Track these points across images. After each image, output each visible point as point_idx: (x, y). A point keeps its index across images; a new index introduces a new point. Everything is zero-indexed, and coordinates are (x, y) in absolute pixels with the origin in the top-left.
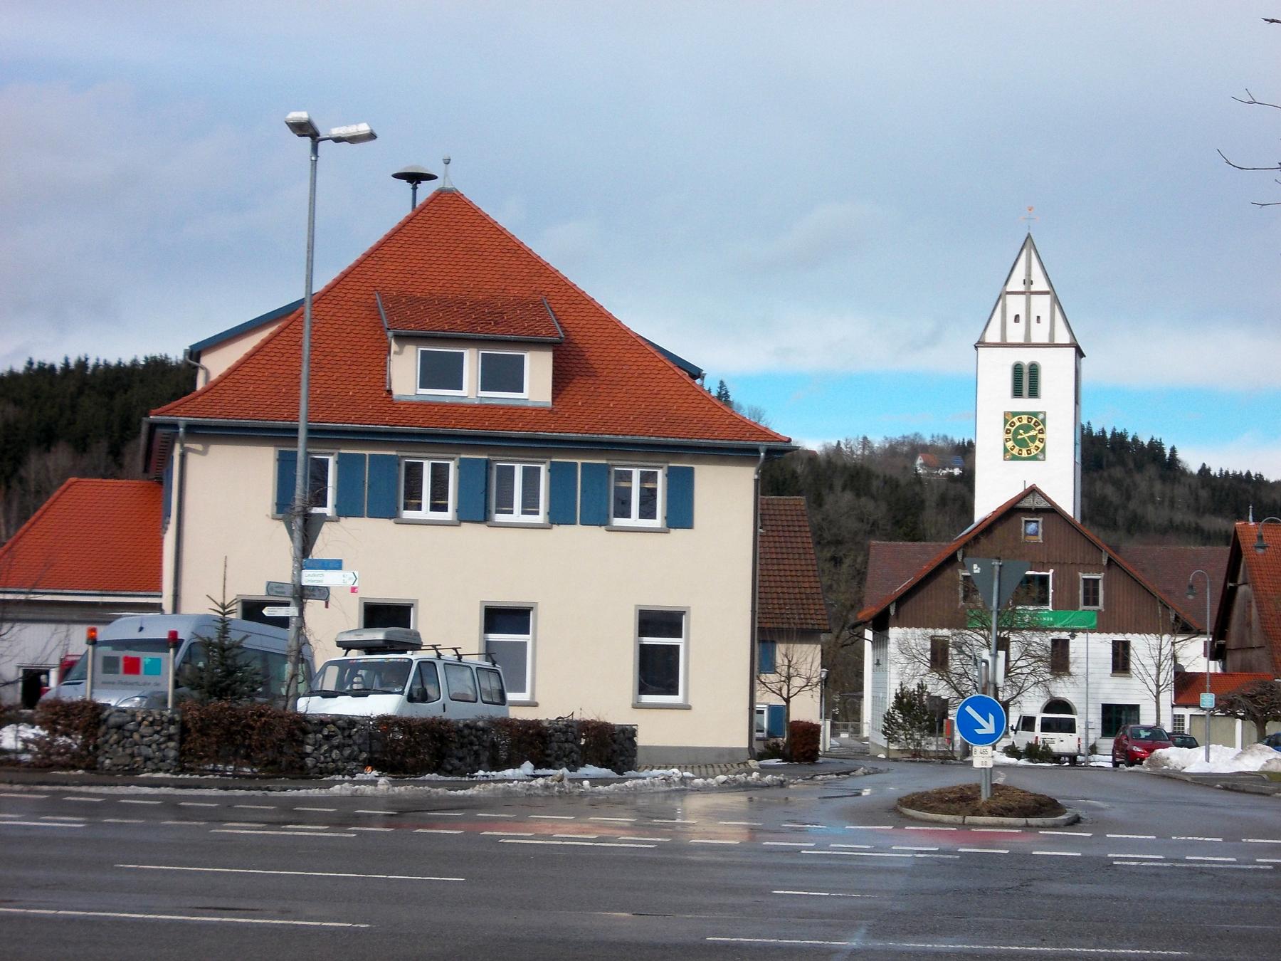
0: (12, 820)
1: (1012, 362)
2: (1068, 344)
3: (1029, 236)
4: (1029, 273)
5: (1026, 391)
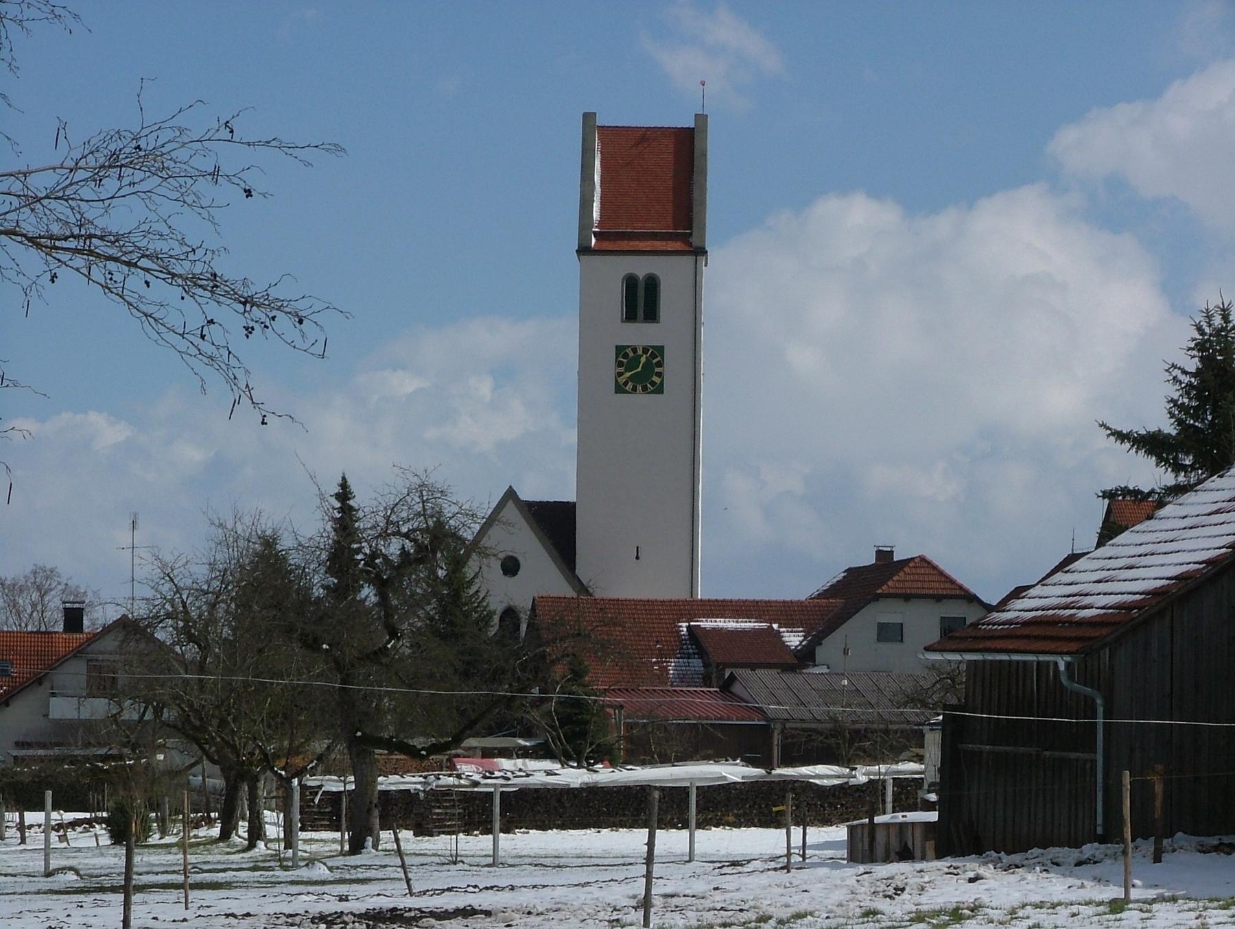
5: (640, 313)
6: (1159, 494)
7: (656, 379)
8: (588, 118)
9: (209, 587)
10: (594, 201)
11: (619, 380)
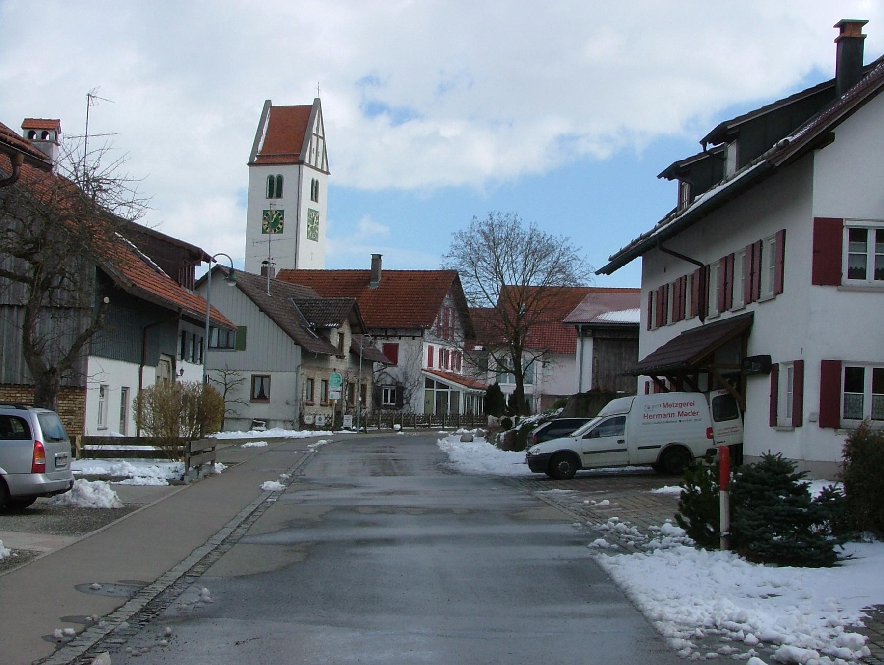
1: (267, 175)
5: (275, 194)
6: (62, 258)
7: (280, 226)
8: (268, 102)
9: (494, 358)
10: (260, 141)
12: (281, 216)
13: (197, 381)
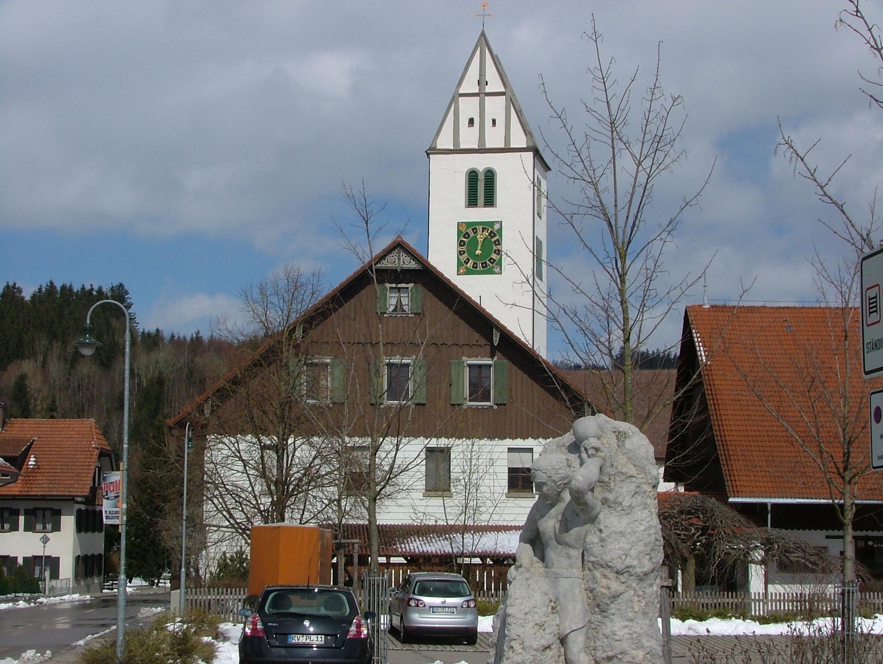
0: (3, 606)
1: (465, 169)
2: (524, 148)
3: (483, 34)
4: (482, 73)
5: (481, 199)
7: (494, 256)
11: (461, 258)
12: (497, 237)
13: (100, 289)
